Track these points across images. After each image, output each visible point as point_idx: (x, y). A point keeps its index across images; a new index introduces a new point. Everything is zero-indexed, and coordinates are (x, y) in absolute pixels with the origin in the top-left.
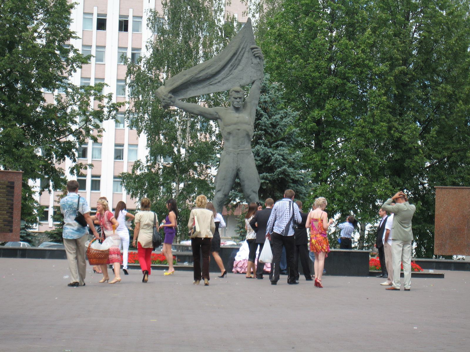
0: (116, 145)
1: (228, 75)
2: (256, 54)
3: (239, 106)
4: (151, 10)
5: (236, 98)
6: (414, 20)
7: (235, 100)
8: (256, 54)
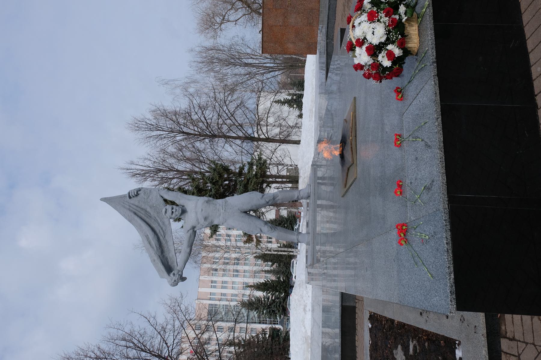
0: (211, 288)
1: (156, 220)
2: (134, 193)
3: (180, 209)
4: (73, 353)
5: (172, 212)
6: (270, 282)
7: (174, 213)
8: (134, 193)
